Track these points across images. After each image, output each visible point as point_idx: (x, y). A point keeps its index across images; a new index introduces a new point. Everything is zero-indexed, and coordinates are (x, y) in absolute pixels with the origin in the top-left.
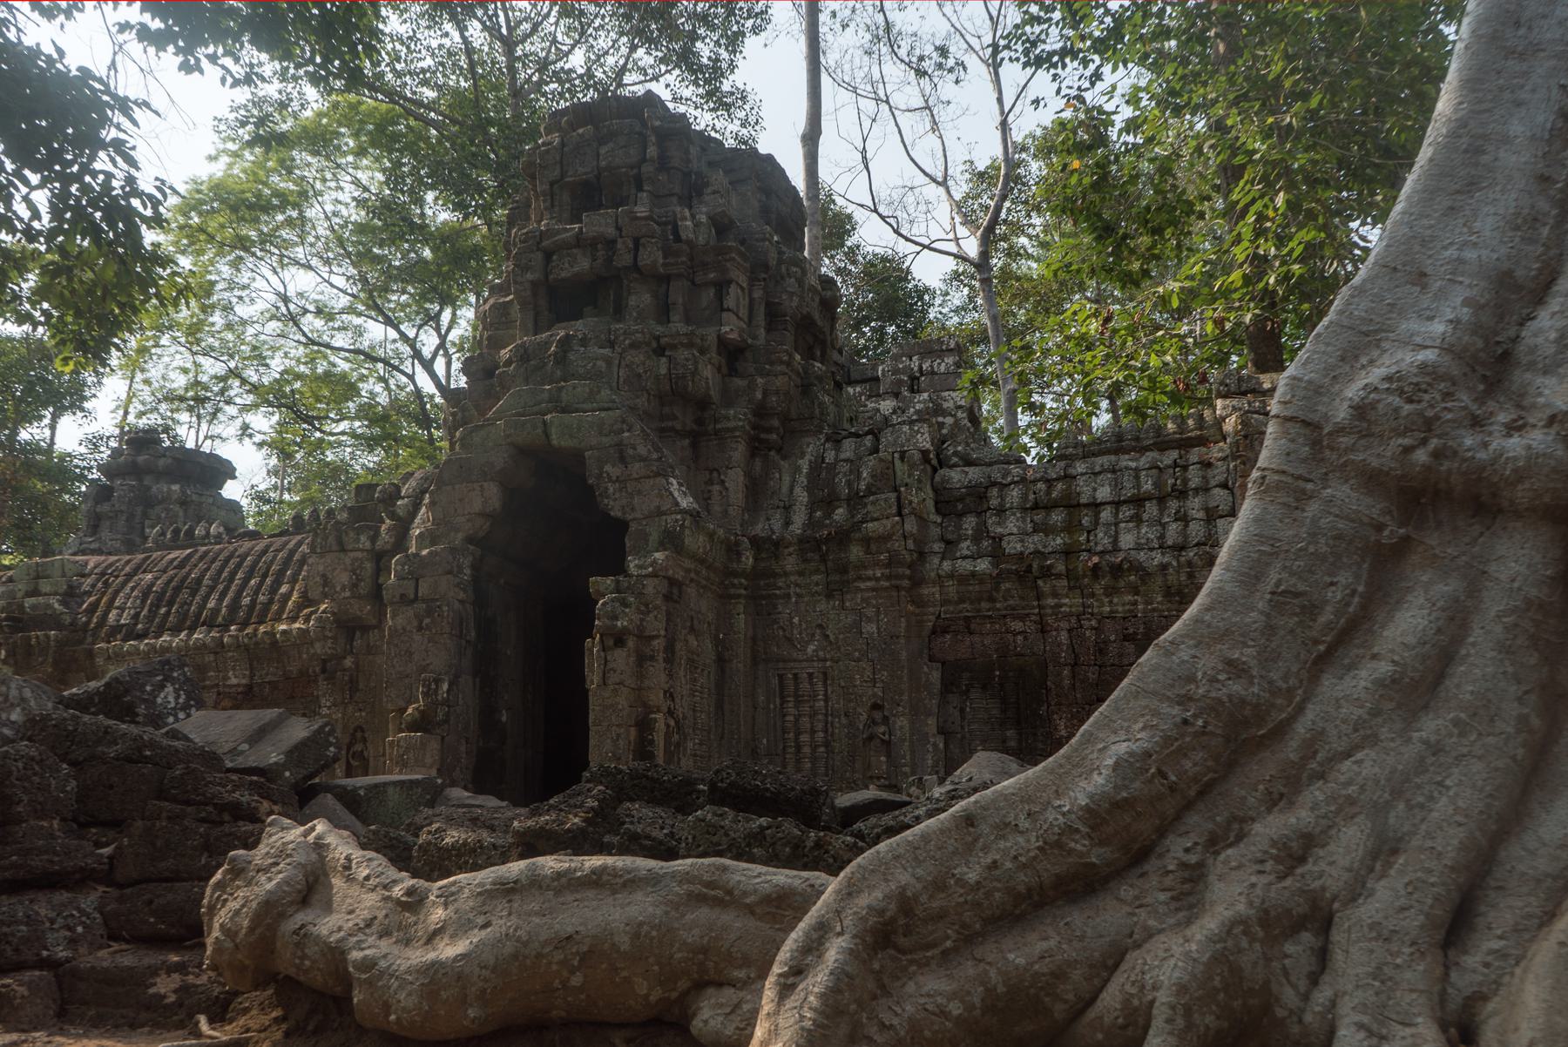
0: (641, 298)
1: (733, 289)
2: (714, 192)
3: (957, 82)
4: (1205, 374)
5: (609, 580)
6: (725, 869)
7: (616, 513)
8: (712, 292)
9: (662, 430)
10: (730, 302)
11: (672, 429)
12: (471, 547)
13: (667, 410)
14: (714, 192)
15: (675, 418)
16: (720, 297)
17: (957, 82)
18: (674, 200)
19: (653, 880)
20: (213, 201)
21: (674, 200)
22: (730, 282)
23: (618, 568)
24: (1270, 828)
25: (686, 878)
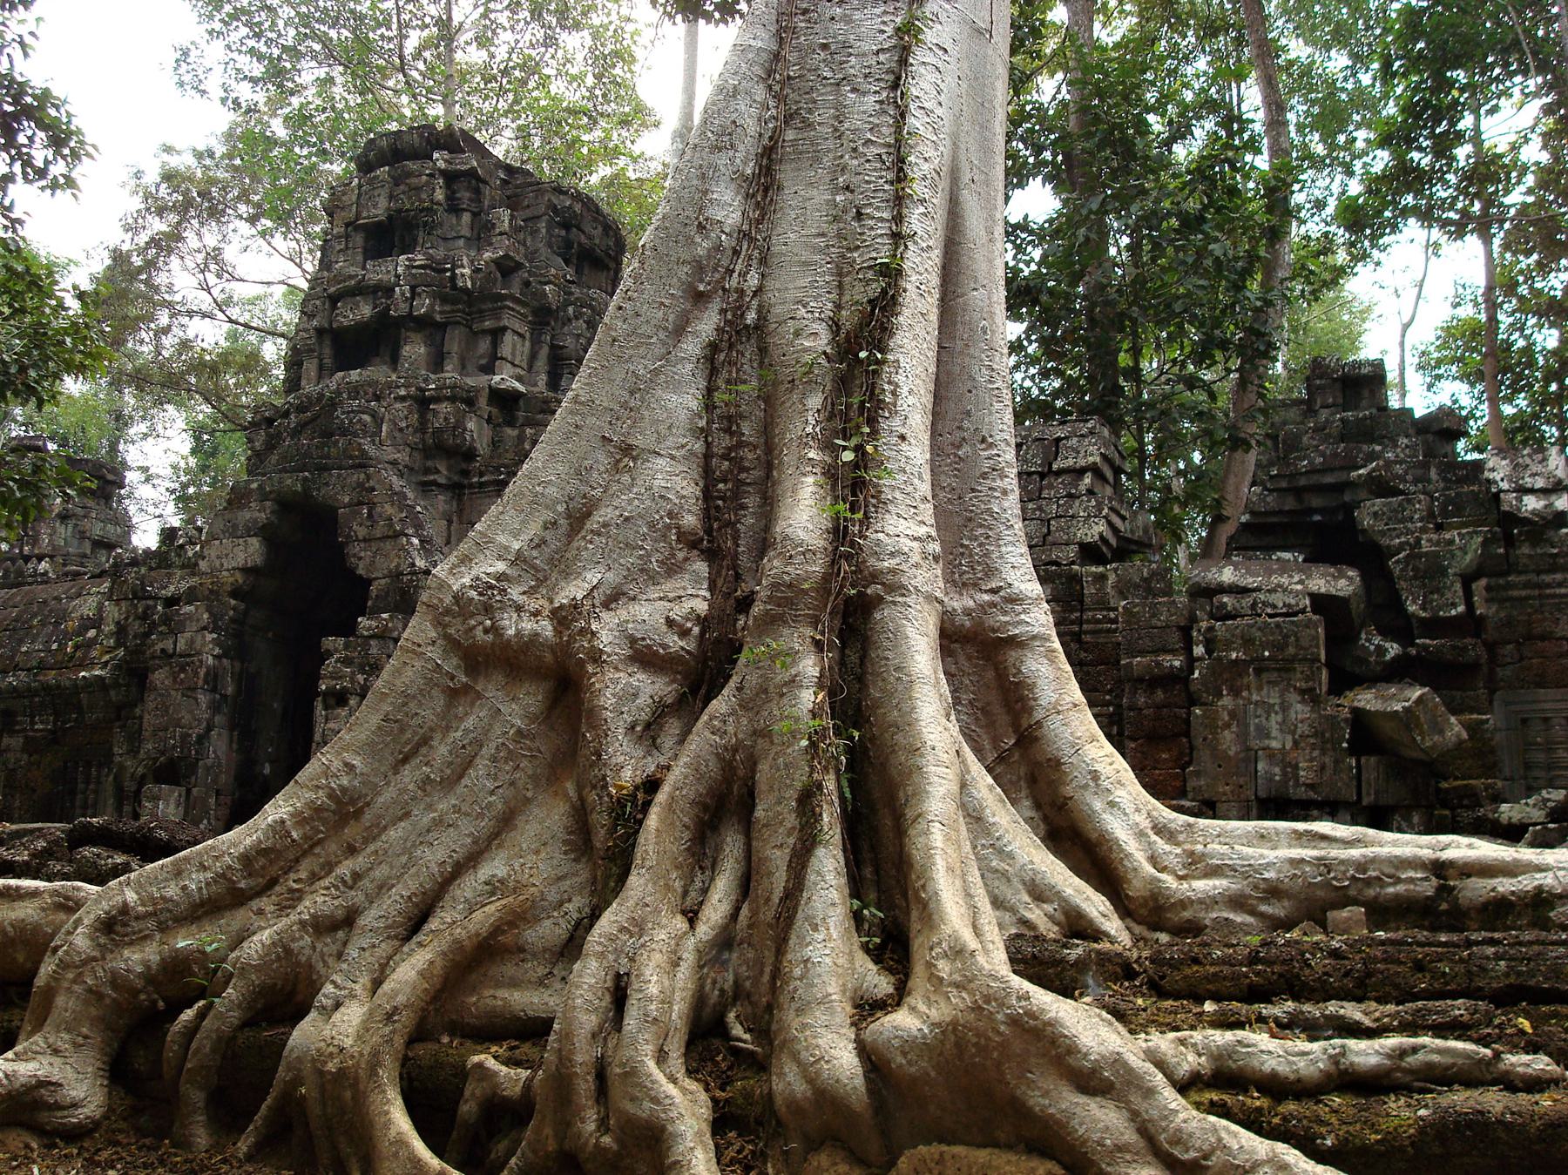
0: (415, 350)
1: (509, 338)
2: (501, 234)
3: (138, 175)
4: (1115, 424)
5: (341, 641)
6: (79, 889)
7: (361, 571)
8: (488, 340)
9: (424, 484)
10: (506, 350)
11: (434, 483)
12: (233, 602)
13: (429, 463)
14: (501, 234)
15: (438, 472)
16: (495, 344)
17: (138, 175)
18: (461, 242)
19: (35, 893)
20: (1277, 151)
21: (461, 242)
22: (505, 329)
23: (348, 629)
24: (345, 869)
25: (56, 893)
